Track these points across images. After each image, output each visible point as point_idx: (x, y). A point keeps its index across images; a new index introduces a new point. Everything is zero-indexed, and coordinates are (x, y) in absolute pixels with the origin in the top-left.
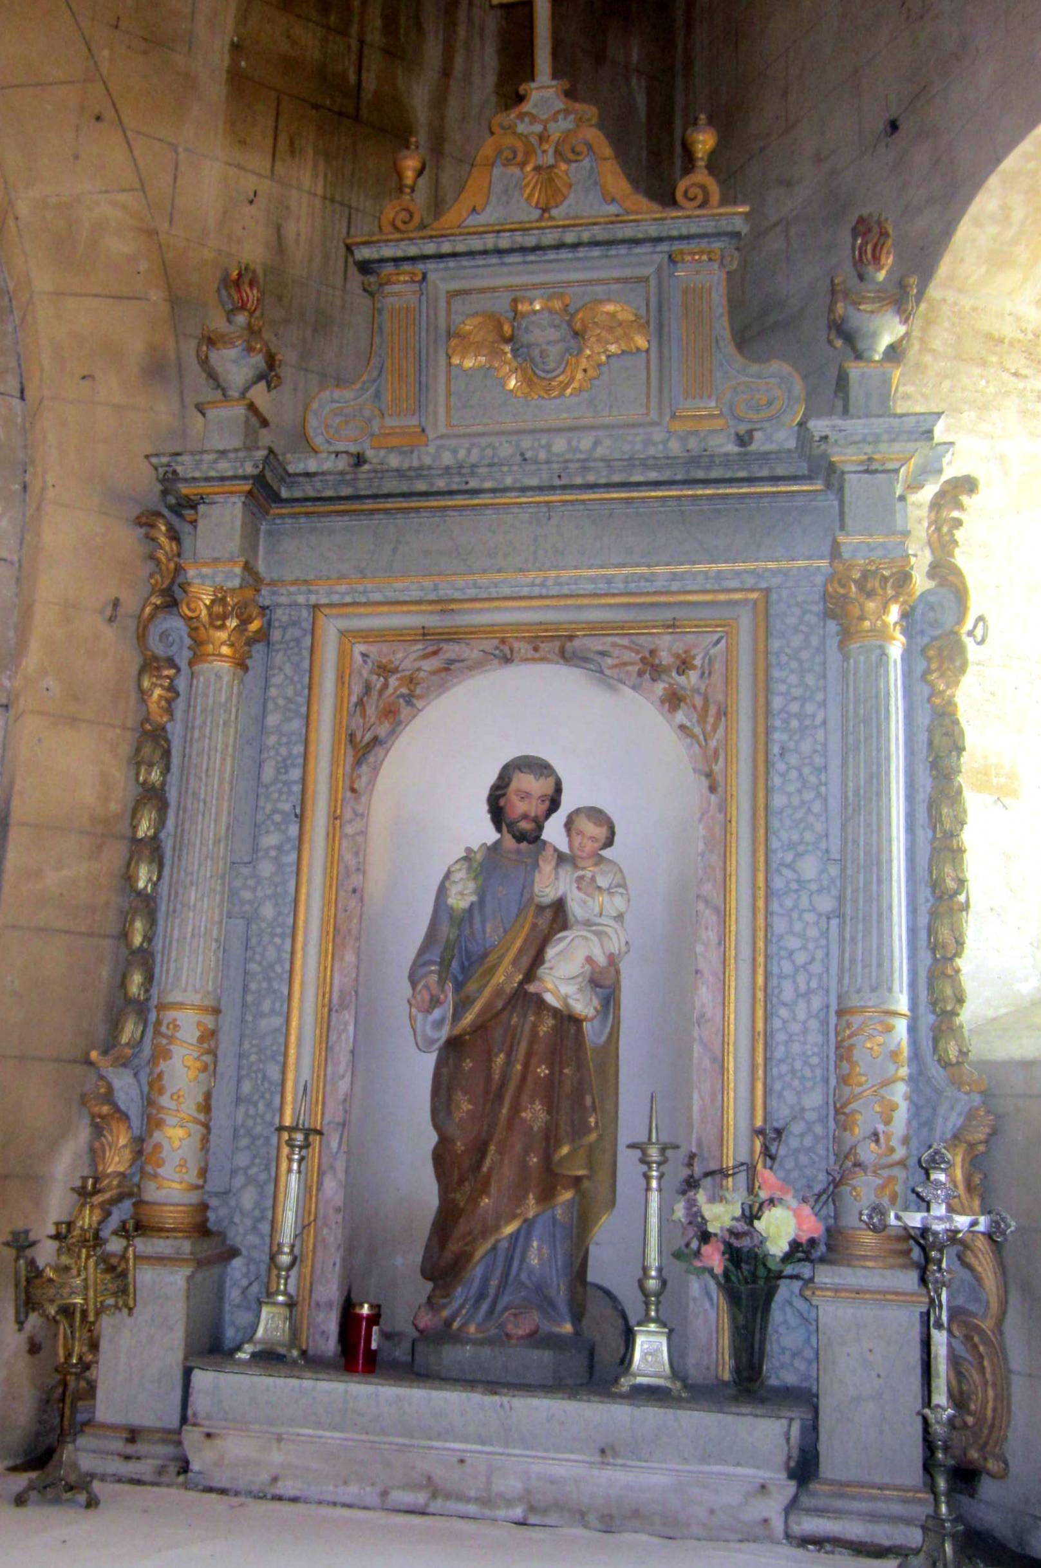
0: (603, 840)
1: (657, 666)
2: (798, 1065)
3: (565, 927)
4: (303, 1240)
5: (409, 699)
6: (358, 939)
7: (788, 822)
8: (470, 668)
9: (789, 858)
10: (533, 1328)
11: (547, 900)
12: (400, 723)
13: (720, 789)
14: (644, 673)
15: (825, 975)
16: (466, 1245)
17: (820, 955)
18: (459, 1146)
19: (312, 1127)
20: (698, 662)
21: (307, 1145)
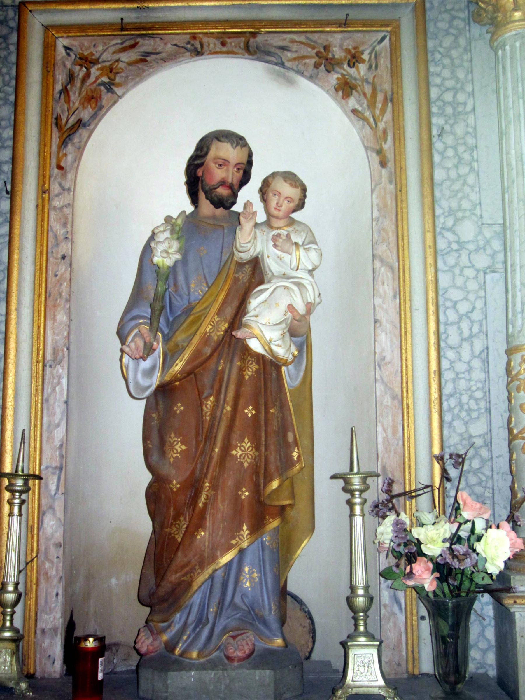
0: (297, 202)
1: (331, 59)
2: (465, 399)
3: (262, 282)
4: (26, 575)
5: (110, 87)
6: (68, 300)
7: (447, 193)
8: (164, 60)
9: (450, 223)
10: (251, 647)
11: (245, 256)
12: (101, 108)
13: (391, 165)
14: (320, 65)
15: (484, 322)
16: (185, 575)
17: (479, 304)
18: (175, 484)
19: (31, 472)
20: (366, 56)
21: (27, 490)
